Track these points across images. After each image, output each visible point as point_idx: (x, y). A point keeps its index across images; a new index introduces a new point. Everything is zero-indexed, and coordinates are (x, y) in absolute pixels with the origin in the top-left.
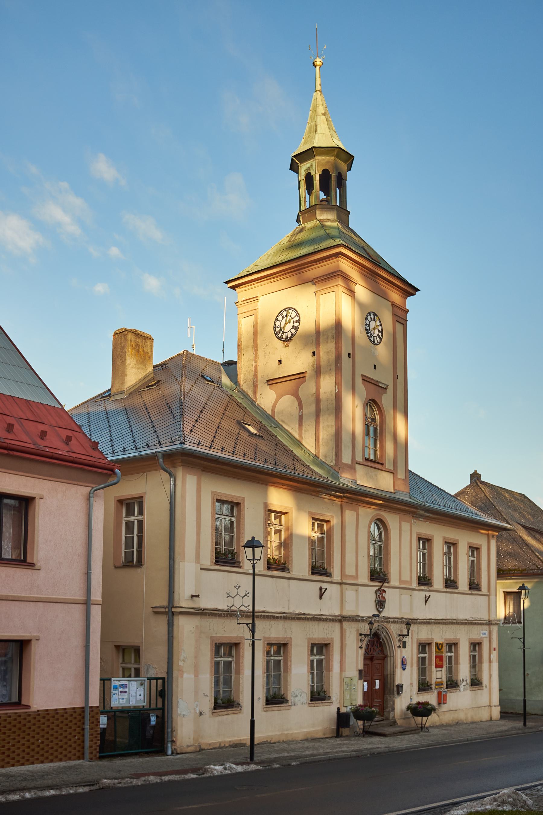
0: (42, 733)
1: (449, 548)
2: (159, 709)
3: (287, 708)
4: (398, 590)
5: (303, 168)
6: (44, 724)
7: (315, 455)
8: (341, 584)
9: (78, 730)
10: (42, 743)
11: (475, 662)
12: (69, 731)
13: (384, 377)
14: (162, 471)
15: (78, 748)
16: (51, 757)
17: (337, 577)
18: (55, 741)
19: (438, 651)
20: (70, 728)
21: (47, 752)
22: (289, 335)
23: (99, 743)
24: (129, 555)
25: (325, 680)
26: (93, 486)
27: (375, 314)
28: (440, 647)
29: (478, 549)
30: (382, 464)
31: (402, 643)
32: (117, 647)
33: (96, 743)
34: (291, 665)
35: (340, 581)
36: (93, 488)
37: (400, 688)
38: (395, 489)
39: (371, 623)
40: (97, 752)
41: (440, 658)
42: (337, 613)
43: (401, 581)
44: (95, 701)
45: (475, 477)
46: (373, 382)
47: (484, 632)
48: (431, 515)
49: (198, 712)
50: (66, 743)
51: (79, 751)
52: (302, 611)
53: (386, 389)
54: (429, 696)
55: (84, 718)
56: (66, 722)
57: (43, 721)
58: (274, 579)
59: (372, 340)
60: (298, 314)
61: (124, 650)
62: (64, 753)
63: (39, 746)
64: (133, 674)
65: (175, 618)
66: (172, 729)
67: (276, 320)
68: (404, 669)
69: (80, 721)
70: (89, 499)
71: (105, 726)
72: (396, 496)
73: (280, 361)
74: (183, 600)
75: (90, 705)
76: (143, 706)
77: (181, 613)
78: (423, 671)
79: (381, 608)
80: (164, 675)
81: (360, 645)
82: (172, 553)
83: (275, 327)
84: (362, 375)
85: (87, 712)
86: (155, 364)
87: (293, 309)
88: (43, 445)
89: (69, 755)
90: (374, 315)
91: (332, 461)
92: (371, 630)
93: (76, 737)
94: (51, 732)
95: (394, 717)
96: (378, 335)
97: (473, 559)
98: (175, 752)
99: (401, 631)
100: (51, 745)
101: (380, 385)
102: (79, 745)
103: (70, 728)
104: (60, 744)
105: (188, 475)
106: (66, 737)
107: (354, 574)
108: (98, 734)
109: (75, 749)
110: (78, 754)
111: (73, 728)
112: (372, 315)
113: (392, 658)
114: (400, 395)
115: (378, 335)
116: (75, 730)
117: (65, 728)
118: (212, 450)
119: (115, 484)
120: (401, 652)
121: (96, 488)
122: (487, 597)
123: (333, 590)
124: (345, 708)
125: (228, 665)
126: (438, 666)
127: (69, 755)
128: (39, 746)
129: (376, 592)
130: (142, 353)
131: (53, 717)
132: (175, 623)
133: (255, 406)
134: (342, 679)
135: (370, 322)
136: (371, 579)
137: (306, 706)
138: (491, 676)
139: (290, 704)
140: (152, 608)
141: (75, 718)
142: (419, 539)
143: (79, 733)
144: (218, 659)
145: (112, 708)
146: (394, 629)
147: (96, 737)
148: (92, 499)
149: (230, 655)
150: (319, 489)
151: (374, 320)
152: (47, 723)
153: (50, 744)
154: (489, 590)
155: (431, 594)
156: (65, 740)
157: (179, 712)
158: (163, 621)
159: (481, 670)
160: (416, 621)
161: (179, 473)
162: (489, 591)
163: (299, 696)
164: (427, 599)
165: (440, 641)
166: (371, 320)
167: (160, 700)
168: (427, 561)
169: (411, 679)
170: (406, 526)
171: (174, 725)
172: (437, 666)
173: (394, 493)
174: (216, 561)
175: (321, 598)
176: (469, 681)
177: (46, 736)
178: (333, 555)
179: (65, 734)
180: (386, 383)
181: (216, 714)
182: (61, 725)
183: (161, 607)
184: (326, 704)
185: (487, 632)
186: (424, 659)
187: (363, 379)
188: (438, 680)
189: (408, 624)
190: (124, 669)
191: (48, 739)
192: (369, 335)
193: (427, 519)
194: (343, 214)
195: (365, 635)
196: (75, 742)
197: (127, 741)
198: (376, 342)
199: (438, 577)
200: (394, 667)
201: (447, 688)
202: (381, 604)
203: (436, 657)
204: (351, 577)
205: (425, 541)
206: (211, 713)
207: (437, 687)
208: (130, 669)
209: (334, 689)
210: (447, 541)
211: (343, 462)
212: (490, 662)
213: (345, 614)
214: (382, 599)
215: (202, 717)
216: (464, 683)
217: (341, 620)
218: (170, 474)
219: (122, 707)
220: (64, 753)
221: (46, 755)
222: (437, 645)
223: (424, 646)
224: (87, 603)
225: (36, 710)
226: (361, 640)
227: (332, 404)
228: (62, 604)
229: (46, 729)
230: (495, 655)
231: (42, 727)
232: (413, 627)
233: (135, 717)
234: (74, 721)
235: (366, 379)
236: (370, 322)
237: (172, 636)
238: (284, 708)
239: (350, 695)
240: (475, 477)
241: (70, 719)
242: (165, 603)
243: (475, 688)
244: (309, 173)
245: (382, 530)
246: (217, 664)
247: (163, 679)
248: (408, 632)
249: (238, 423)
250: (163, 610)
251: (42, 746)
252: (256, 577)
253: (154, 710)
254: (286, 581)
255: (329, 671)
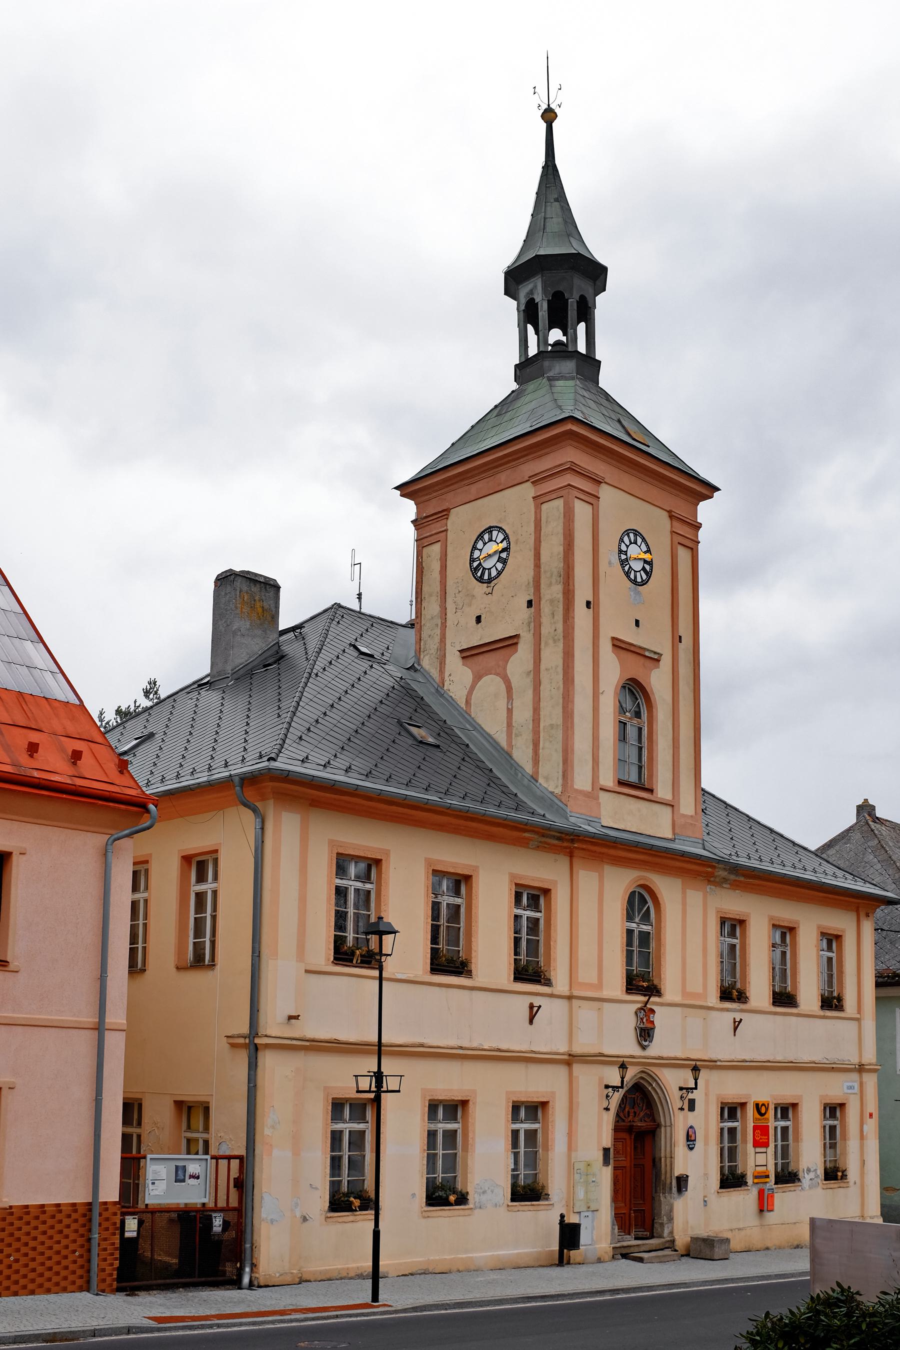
0: (16, 1245)
1: (783, 935)
2: (234, 1209)
3: (467, 1212)
4: (679, 1009)
5: (523, 291)
6: (20, 1229)
7: (532, 777)
8: (570, 998)
9: (80, 1241)
10: (17, 1261)
11: (832, 1138)
12: (64, 1242)
13: (653, 638)
14: (242, 808)
15: (80, 1272)
16: (31, 1286)
17: (561, 983)
18: (40, 1259)
19: (759, 1116)
20: (67, 1237)
21: (25, 1276)
22: (494, 573)
23: (117, 1264)
24: (198, 949)
25: (540, 1165)
26: (110, 831)
27: (636, 533)
28: (763, 1110)
29: (838, 937)
30: (651, 791)
31: (686, 1102)
32: (179, 1104)
33: (112, 1264)
34: (473, 1139)
35: (567, 994)
36: (112, 835)
37: (682, 1182)
38: (674, 834)
39: (623, 1067)
40: (114, 1280)
41: (762, 1131)
42: (563, 1048)
43: (685, 993)
44: (110, 1192)
45: (865, 810)
46: (632, 649)
47: (850, 1084)
48: (742, 879)
49: (298, 1215)
50: (58, 1263)
51: (81, 1277)
52: (494, 1045)
53: (658, 661)
54: (742, 1196)
55: (90, 1220)
56: (58, 1227)
57: (17, 1223)
58: (444, 989)
59: (632, 576)
60: (506, 537)
61: (190, 1108)
62: (55, 1279)
63: (10, 1267)
64: (201, 1151)
65: (260, 1054)
66: (252, 1244)
67: (474, 548)
68: (691, 1149)
69: (84, 1226)
70: (105, 855)
71: (135, 1234)
72: (677, 846)
73: (479, 619)
74: (273, 1025)
75: (101, 1200)
76: (204, 1204)
77: (267, 1046)
78: (730, 1151)
79: (646, 1041)
80: (242, 1152)
81: (605, 1105)
82: (257, 946)
83: (472, 560)
84: (613, 639)
85: (96, 1211)
86: (281, 627)
87: (500, 529)
88: (29, 767)
89: (63, 1284)
90: (635, 535)
91: (557, 787)
92: (623, 1078)
93: (77, 1254)
94: (32, 1244)
95: (671, 1233)
96: (644, 569)
97: (830, 954)
98: (256, 1283)
99: (686, 1081)
100: (32, 1265)
101: (647, 654)
102: (82, 1267)
103: (67, 1237)
104: (48, 1263)
105: (284, 814)
106: (58, 1253)
107: (595, 981)
108: (116, 1249)
109: (74, 1272)
110: (79, 1282)
111: (71, 1238)
112: (632, 535)
113: (668, 1129)
114: (685, 670)
115: (644, 569)
116: (75, 1241)
117: (57, 1237)
118: (329, 769)
119: (148, 828)
120: (686, 1118)
121: (116, 836)
122: (855, 1023)
123: (551, 1010)
124: (577, 1216)
125: (451, 1136)
126: (760, 1143)
127: (63, 1284)
128: (10, 1267)
129: (636, 1013)
130: (260, 610)
131: (37, 1218)
132: (259, 1064)
133: (442, 696)
134: (571, 1167)
135: (627, 547)
136: (627, 989)
137: (503, 1209)
138: (863, 1163)
139: (471, 1206)
140: (227, 1037)
141: (76, 1221)
142: (723, 921)
143: (82, 1246)
144: (516, 1126)
145: (147, 1205)
146: (672, 1081)
147: (112, 1254)
148: (109, 854)
149: (535, 1119)
150: (527, 835)
151: (636, 543)
152: (26, 1229)
153: (30, 1263)
154: (859, 1011)
155: (745, 1016)
156: (56, 1258)
157: (264, 1215)
158: (242, 1058)
159: (844, 1153)
160: (714, 1065)
161: (270, 809)
162: (859, 1012)
163: (489, 1192)
164: (736, 1025)
165: (761, 1099)
166: (631, 543)
167: (233, 1192)
168: (733, 958)
169: (705, 1165)
170: (695, 897)
171: (255, 1237)
172: (756, 1144)
173: (673, 840)
174: (335, 959)
175: (531, 1022)
176: (821, 1172)
177: (24, 1250)
178: (555, 948)
179: (56, 1247)
180: (658, 651)
181: (334, 1220)
182: (17, 1234)
183: (239, 1036)
184: (542, 1207)
185: (856, 1085)
186: (732, 1131)
187: (613, 645)
188: (759, 1169)
189: (696, 1069)
190: (189, 1141)
191: (26, 1255)
192: (626, 568)
193: (735, 886)
194: (589, 366)
195: (613, 1087)
196: (75, 1262)
197: (175, 1261)
198: (639, 580)
199: (759, 988)
200: (672, 1145)
201: (776, 1183)
202: (645, 1034)
203: (755, 1128)
204: (590, 986)
205: (733, 926)
206: (323, 1217)
207: (756, 1181)
208: (197, 1140)
209: (556, 1182)
210: (777, 923)
211: (575, 787)
212: (862, 1137)
213: (577, 1049)
214: (649, 1026)
215: (306, 1224)
216: (812, 1175)
217: (570, 1060)
218: (255, 810)
219: (186, 1204)
220: (55, 1279)
221: (22, 1282)
222: (757, 1107)
223: (731, 1110)
224: (100, 1028)
225: (7, 1206)
226: (607, 1096)
227: (558, 688)
228: (57, 1029)
229: (24, 1239)
230: (871, 1127)
231: (17, 1234)
232: (703, 1075)
233: (190, 1220)
234: (74, 1226)
235: (619, 645)
236: (627, 547)
237: (255, 1086)
238: (461, 1212)
239: (586, 1192)
240: (865, 810)
241: (66, 1221)
242: (245, 1030)
243: (832, 1184)
244: (533, 299)
245: (650, 903)
246: (515, 1134)
247: (240, 1158)
248: (696, 1084)
249: (400, 723)
250: (241, 1041)
251: (15, 1266)
252: (384, 982)
253: (221, 1210)
254: (466, 992)
255: (548, 1151)
